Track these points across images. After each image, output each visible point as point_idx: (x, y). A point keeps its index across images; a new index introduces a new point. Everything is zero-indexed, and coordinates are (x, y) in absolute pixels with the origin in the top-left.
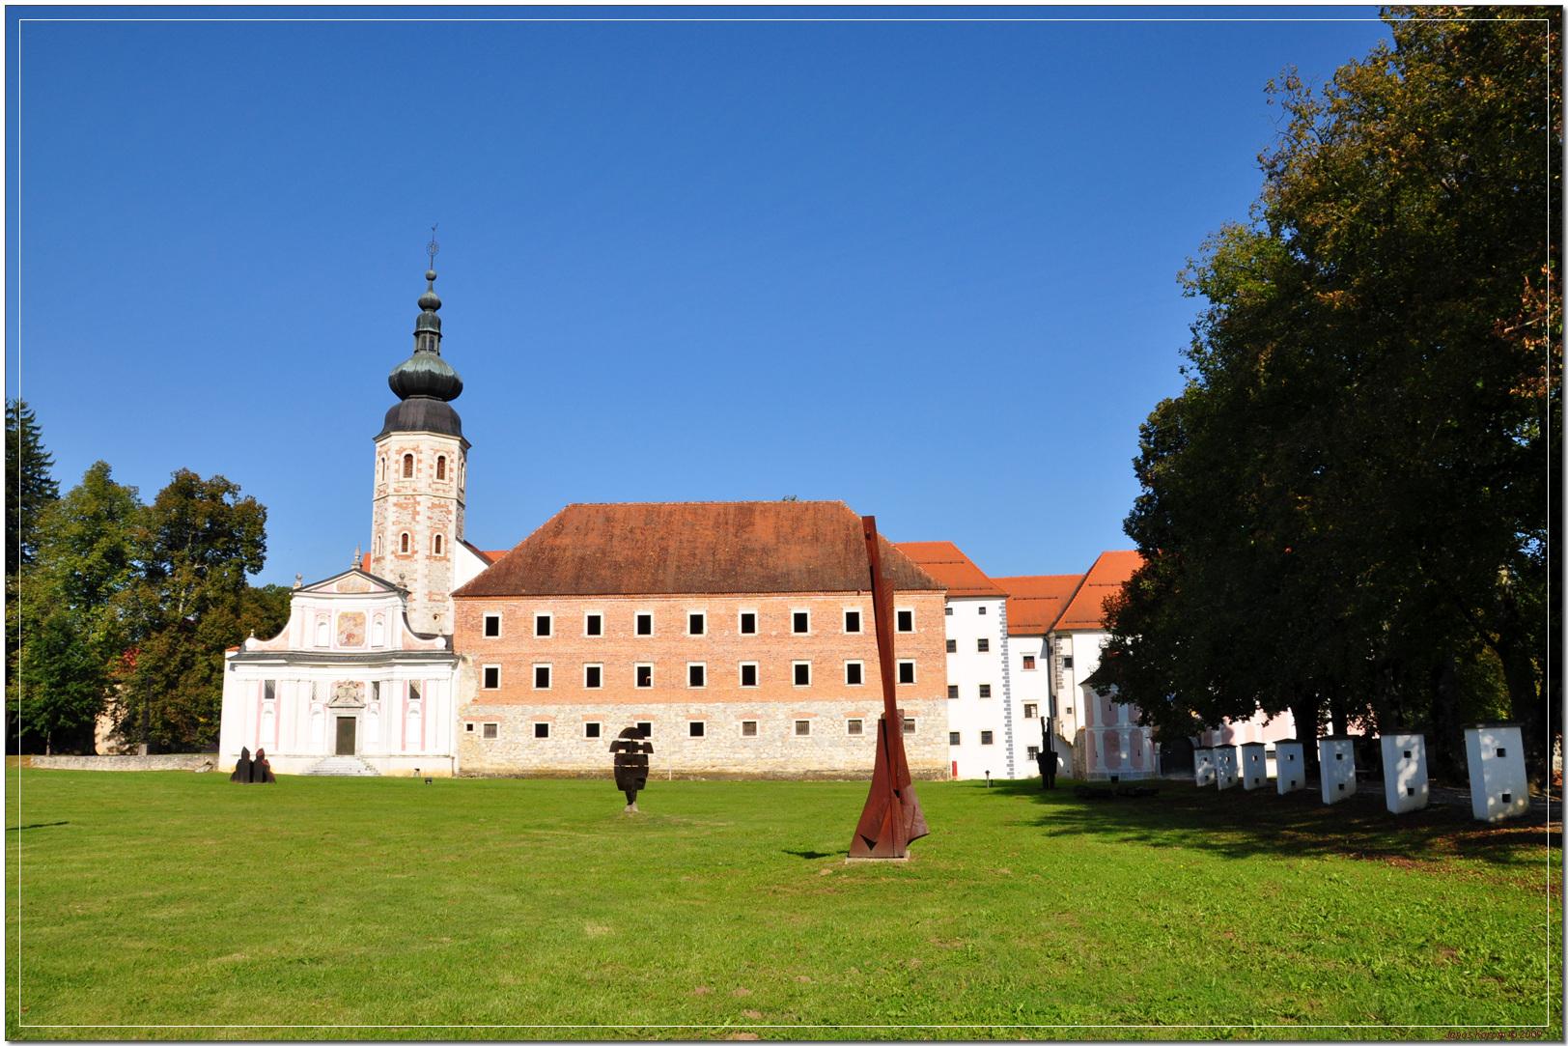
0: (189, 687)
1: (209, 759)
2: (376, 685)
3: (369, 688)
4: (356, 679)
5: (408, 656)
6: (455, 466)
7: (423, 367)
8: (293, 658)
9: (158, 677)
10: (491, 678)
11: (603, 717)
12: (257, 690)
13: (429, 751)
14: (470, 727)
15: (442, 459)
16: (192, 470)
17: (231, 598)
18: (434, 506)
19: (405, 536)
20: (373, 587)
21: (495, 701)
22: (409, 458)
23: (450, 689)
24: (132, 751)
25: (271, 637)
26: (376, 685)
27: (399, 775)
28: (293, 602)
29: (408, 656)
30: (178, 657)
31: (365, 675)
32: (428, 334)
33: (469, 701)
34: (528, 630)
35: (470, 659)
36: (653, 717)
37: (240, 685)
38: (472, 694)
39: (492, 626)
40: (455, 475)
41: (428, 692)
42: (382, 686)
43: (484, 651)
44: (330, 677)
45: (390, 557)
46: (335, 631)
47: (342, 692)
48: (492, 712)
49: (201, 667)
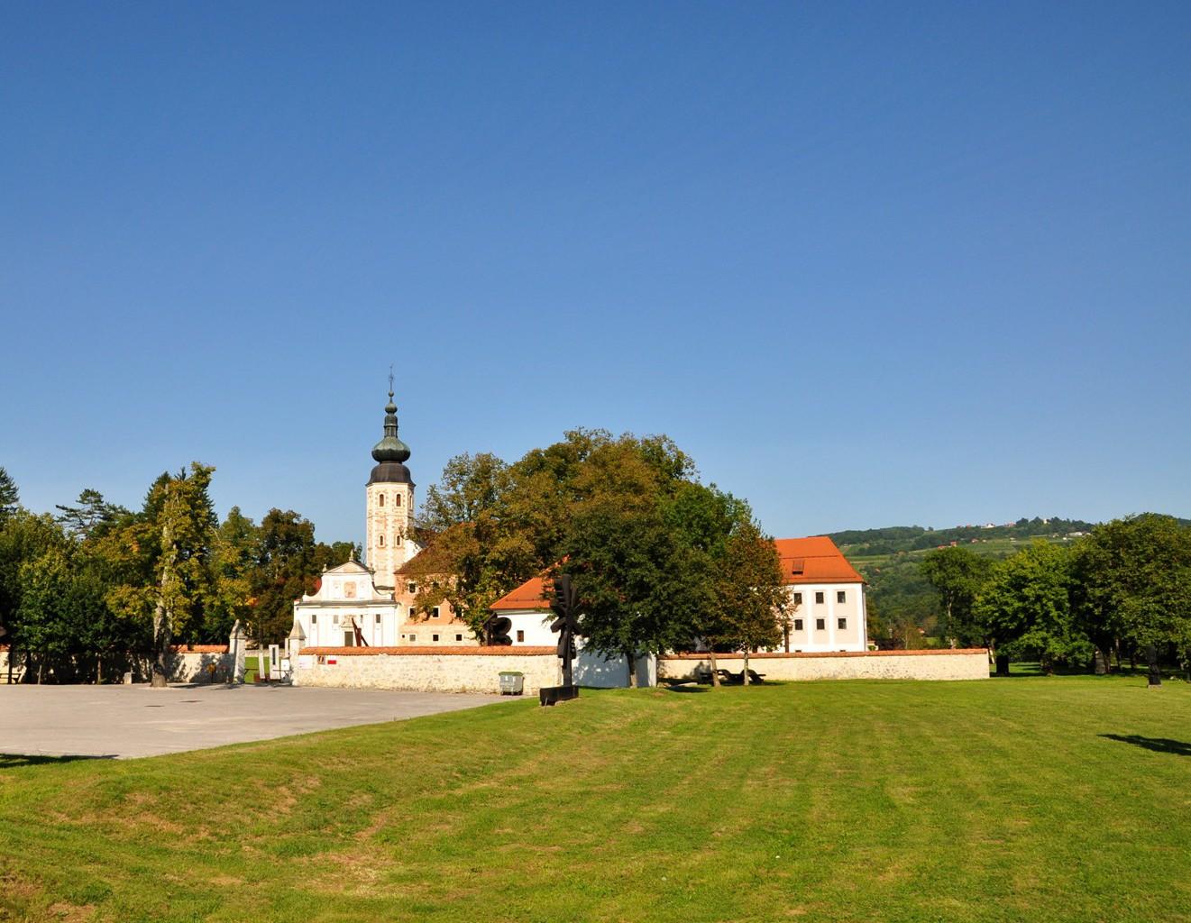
0: (281, 617)
2: (362, 616)
5: (375, 603)
6: (406, 499)
7: (387, 447)
8: (324, 604)
9: (267, 612)
11: (441, 632)
14: (403, 636)
15: (399, 496)
17: (299, 572)
18: (395, 521)
19: (382, 537)
22: (382, 496)
24: (257, 648)
26: (362, 616)
29: (375, 603)
30: (276, 602)
31: (356, 611)
32: (391, 425)
36: (416, 632)
37: (301, 615)
40: (406, 503)
44: (342, 612)
45: (374, 548)
46: (343, 591)
49: (287, 606)
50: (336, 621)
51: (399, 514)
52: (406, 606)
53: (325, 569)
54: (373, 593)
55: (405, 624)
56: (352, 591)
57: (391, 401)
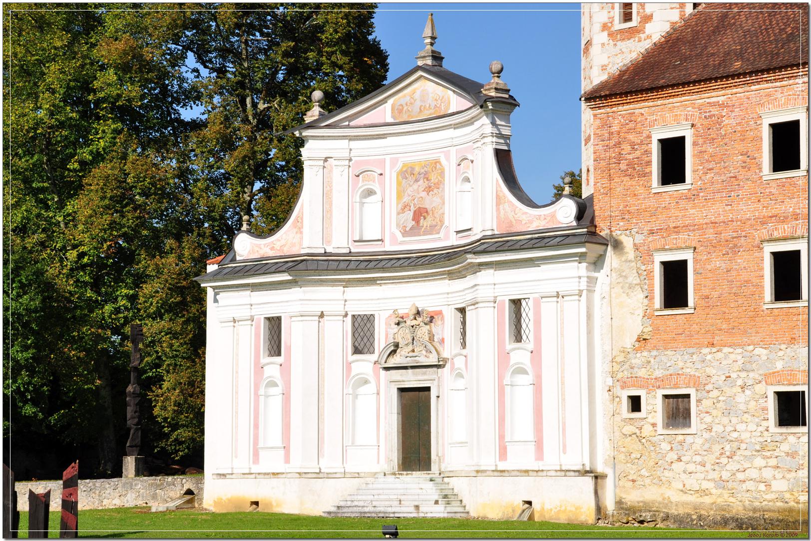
1: (186, 482)
3: (451, 319)
4: (428, 305)
5: (503, 247)
8: (303, 269)
10: (675, 279)
12: (251, 337)
14: (635, 403)
20: (456, 101)
23: (591, 310)
25: (272, 232)
27: (494, 514)
28: (306, 152)
29: (503, 247)
33: (629, 341)
34: (750, 161)
35: (627, 242)
38: (635, 326)
41: (543, 319)
42: (527, 311)
43: (649, 223)
48: (677, 365)
50: (362, 334)
52: (644, 254)
53: (315, 112)
54: (499, 200)
55: (642, 340)
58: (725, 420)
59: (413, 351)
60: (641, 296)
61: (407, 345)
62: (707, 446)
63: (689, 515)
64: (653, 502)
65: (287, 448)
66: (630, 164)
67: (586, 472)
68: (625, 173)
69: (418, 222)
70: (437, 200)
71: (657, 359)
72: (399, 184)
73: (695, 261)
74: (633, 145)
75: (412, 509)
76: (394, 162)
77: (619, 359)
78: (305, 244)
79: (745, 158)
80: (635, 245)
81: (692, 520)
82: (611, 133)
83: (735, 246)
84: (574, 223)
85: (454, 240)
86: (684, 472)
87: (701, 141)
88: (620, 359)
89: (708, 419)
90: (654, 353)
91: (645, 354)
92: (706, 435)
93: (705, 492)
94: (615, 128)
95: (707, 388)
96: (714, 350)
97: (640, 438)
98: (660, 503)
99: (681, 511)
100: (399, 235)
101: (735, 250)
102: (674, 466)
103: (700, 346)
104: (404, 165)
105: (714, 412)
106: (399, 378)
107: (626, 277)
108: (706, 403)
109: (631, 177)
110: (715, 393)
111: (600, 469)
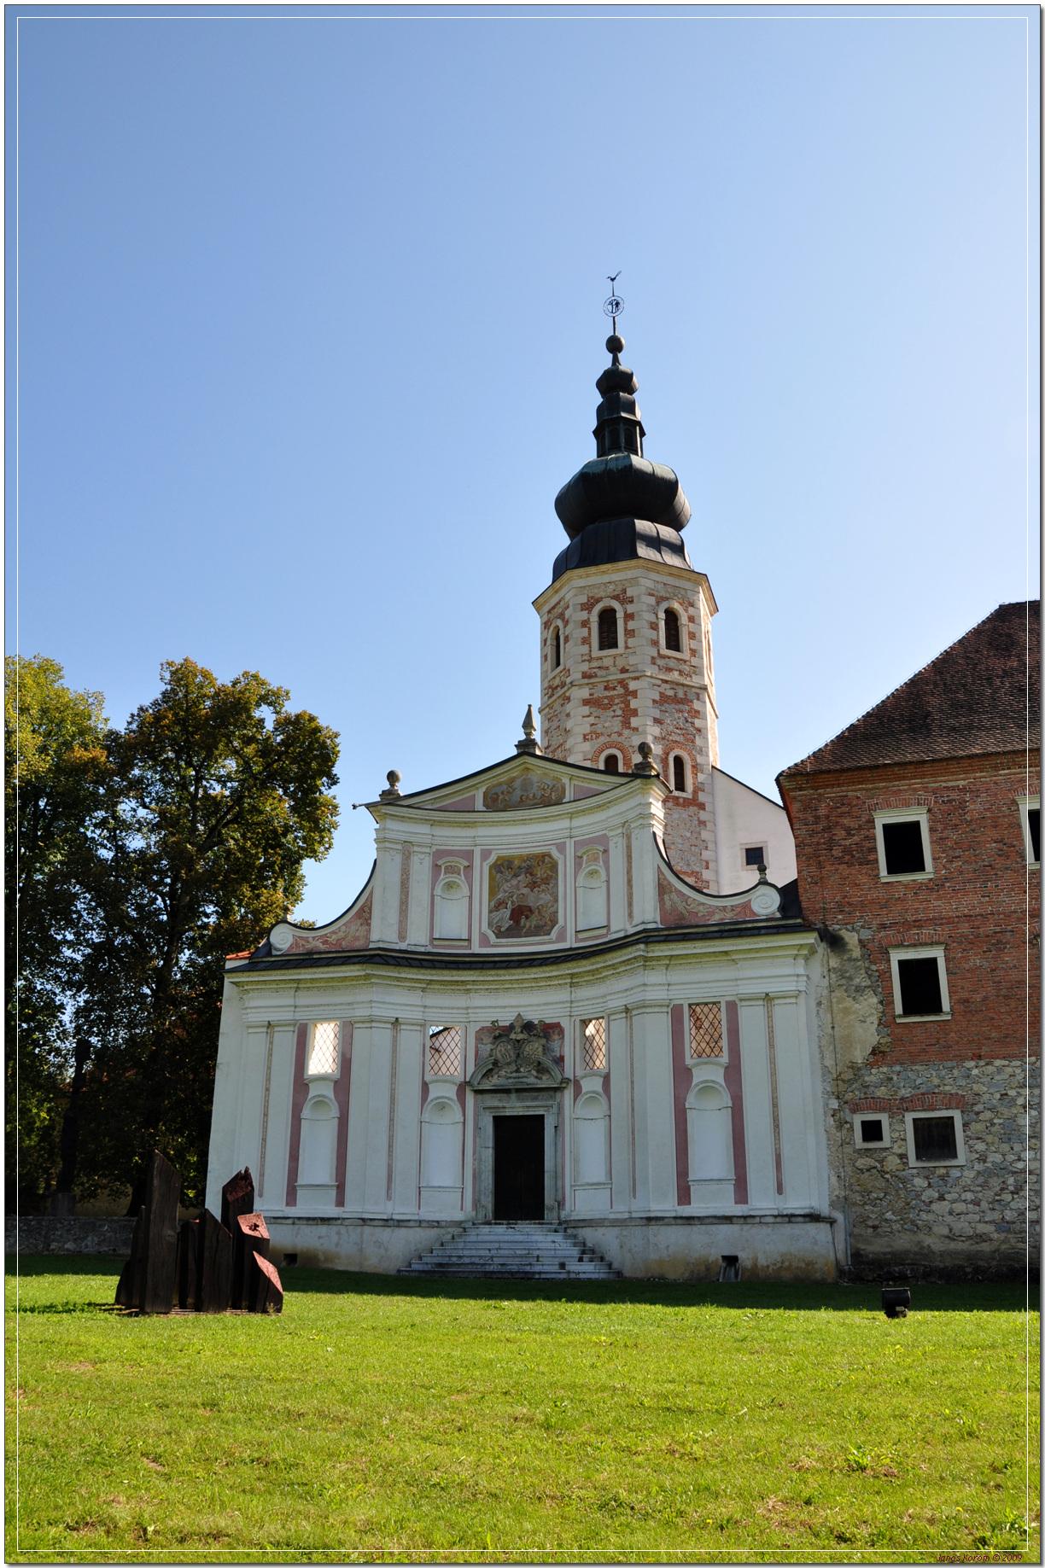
4: (534, 1016)
10: (920, 985)
13: (762, 1201)
14: (872, 1131)
16: (201, 663)
21: (943, 1049)
22: (607, 618)
33: (859, 1055)
35: (851, 939)
38: (868, 1035)
39: (904, 847)
47: (504, 1050)
51: (675, 676)
56: (535, 899)
57: (615, 360)
58: (1005, 1147)
59: (517, 1071)
60: (875, 1000)
61: (509, 1064)
62: (981, 1180)
63: (961, 1267)
64: (907, 1252)
65: (341, 1188)
66: (847, 851)
67: (814, 1218)
68: (840, 860)
69: (517, 922)
70: (545, 897)
71: (903, 1075)
72: (492, 878)
73: (947, 960)
74: (849, 832)
75: (556, 1268)
76: (485, 854)
77: (846, 1077)
78: (374, 936)
79: (1000, 845)
80: (860, 941)
81: (966, 1274)
82: (817, 817)
83: (999, 942)
84: (778, 915)
85: (570, 943)
86: (951, 1213)
87: (940, 827)
88: (848, 1075)
89: (981, 1146)
90: (898, 1068)
91: (885, 1069)
92: (978, 1167)
93: (982, 1238)
94: (822, 812)
95: (976, 1108)
96: (982, 1063)
97: (882, 1172)
98: (916, 1253)
99: (948, 1263)
100: (492, 937)
101: (1000, 946)
102: (934, 1207)
103: (963, 1058)
104: (499, 858)
105: (989, 1138)
106: (496, 1104)
107: (850, 978)
108: (976, 1127)
109: (850, 865)
110: (988, 1115)
111: (825, 1210)
